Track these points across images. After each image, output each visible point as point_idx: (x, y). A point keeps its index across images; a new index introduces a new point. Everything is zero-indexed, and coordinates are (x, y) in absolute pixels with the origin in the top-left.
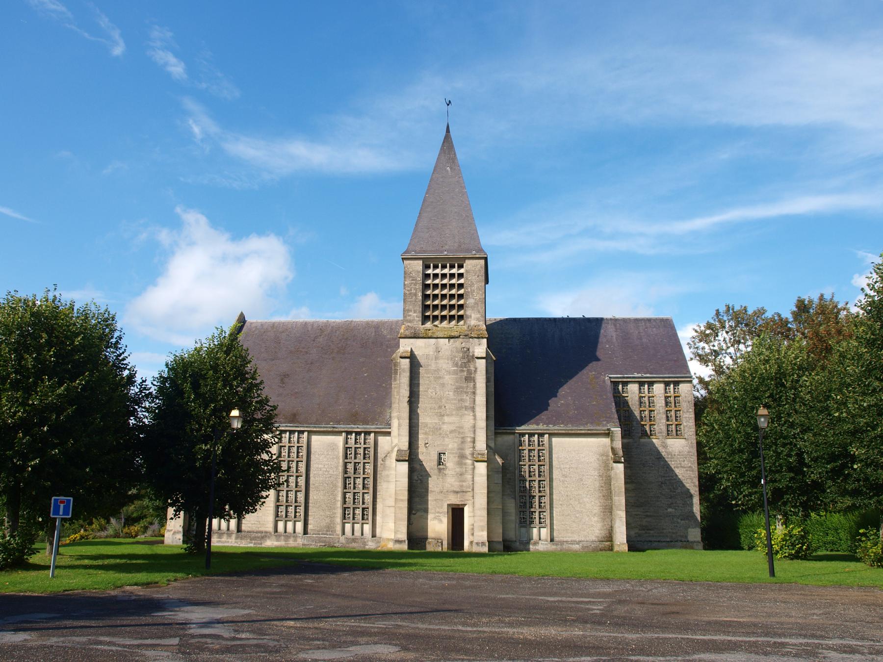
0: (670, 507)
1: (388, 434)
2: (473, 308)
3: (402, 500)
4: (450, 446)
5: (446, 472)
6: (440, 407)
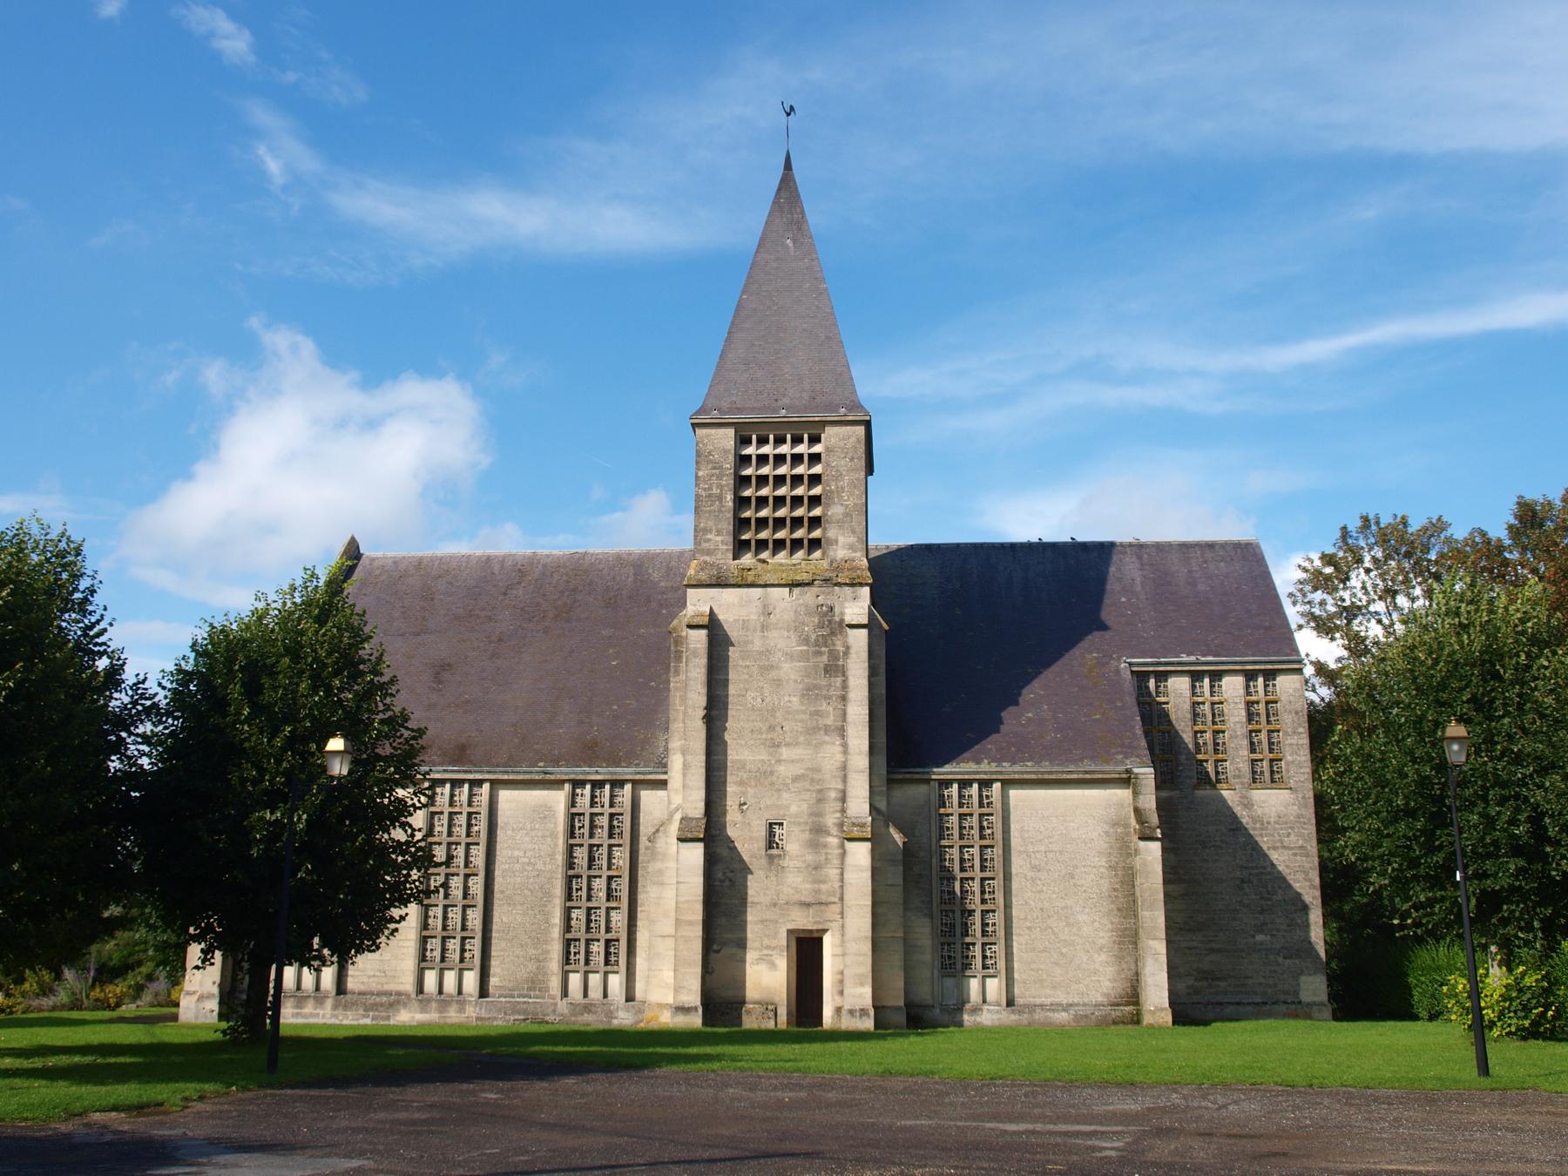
0: (1261, 932)
1: (662, 784)
2: (840, 523)
3: (690, 923)
4: (794, 809)
5: (785, 863)
6: (771, 728)
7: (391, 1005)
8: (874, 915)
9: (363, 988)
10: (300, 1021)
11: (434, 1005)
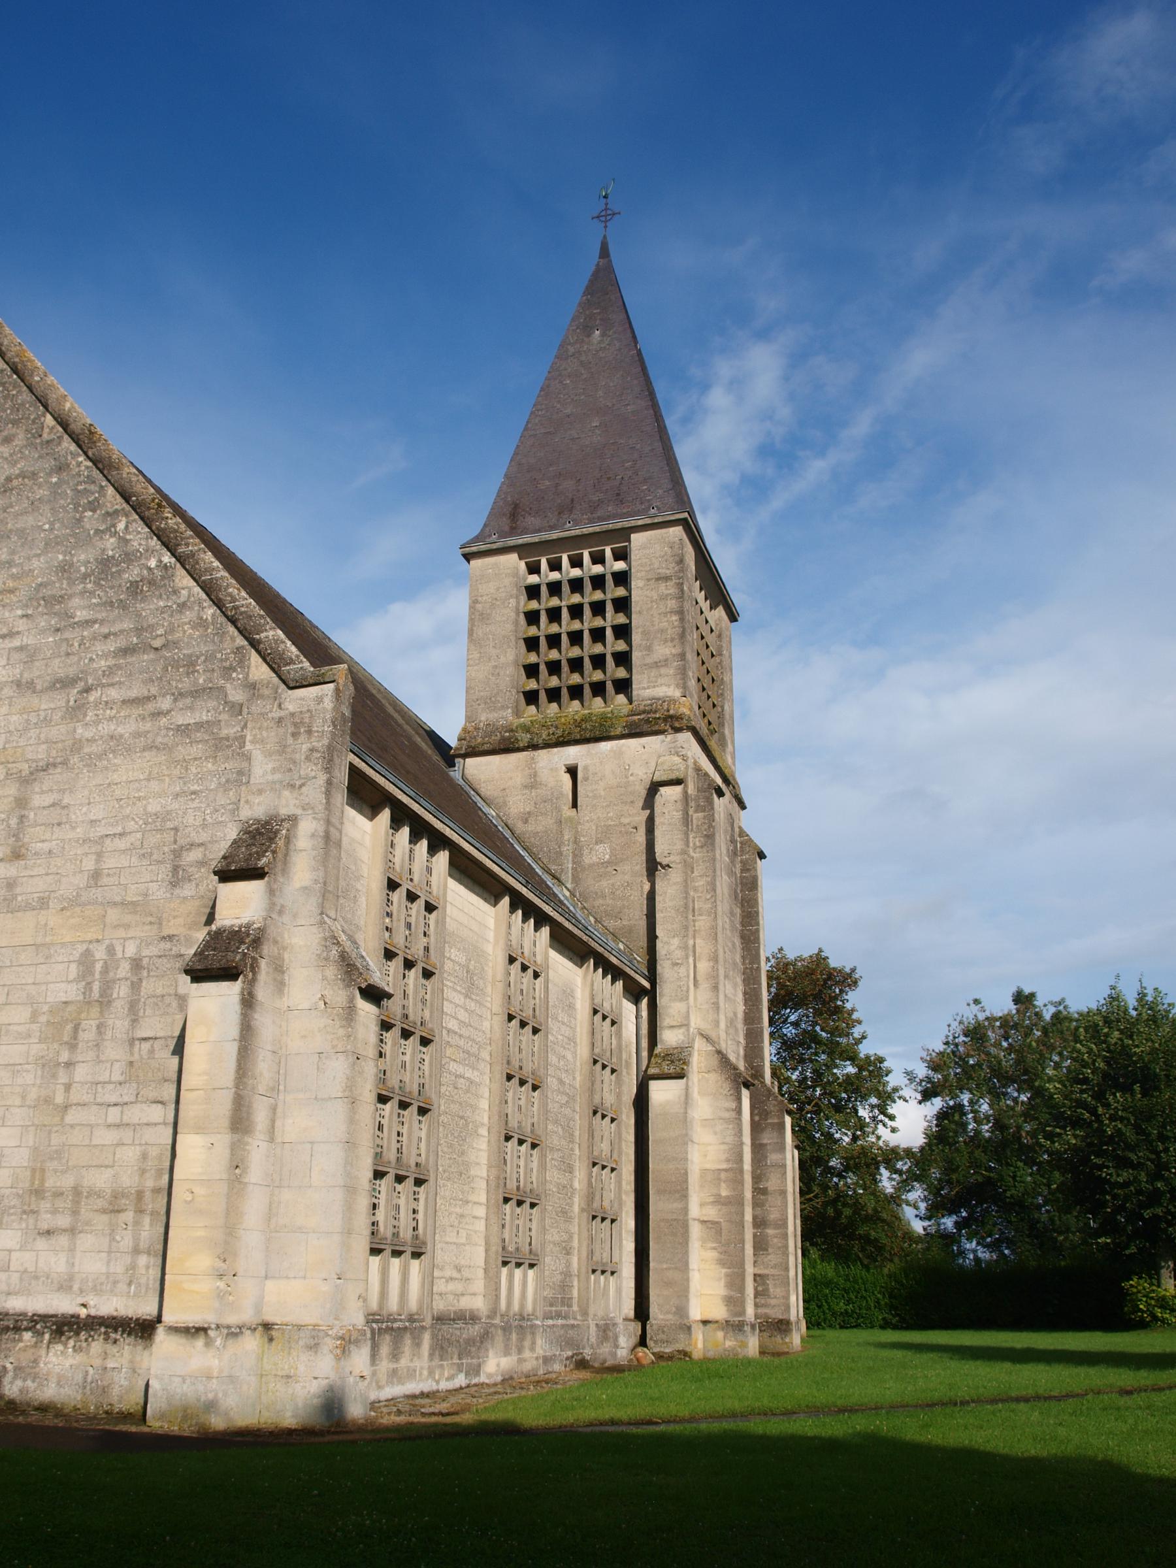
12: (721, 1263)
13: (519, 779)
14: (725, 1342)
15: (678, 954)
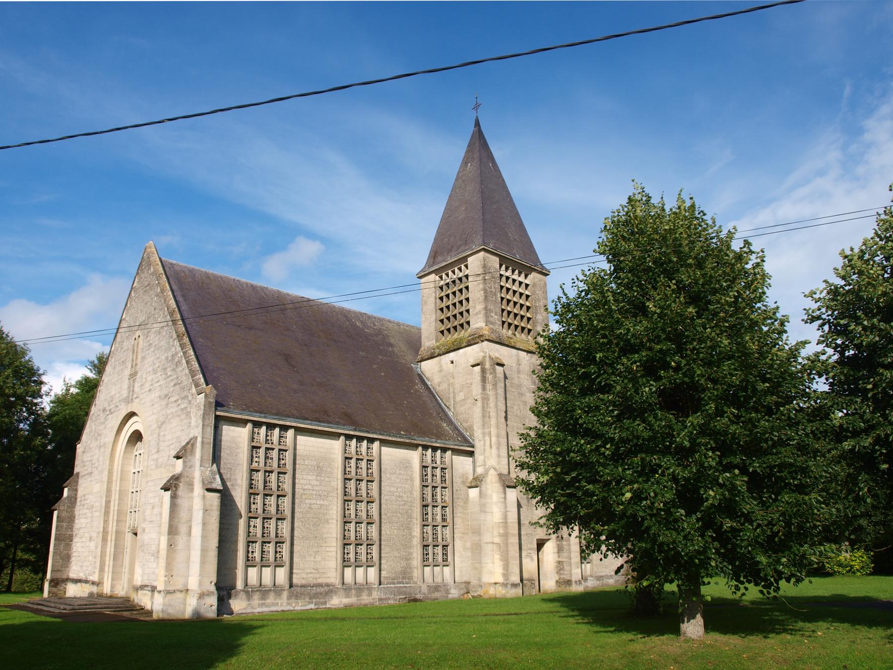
7: (327, 593)
8: (220, 535)
9: (304, 582)
10: (265, 609)
11: (353, 591)
12: (501, 560)
13: (437, 369)
14: (500, 592)
15: (481, 436)
